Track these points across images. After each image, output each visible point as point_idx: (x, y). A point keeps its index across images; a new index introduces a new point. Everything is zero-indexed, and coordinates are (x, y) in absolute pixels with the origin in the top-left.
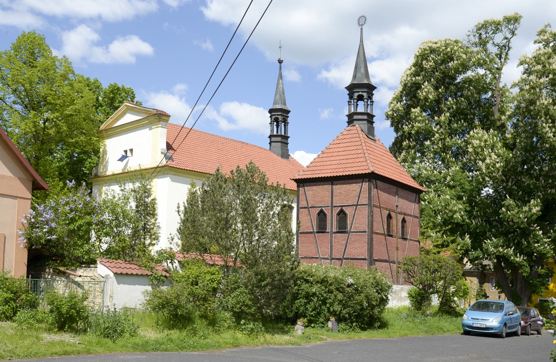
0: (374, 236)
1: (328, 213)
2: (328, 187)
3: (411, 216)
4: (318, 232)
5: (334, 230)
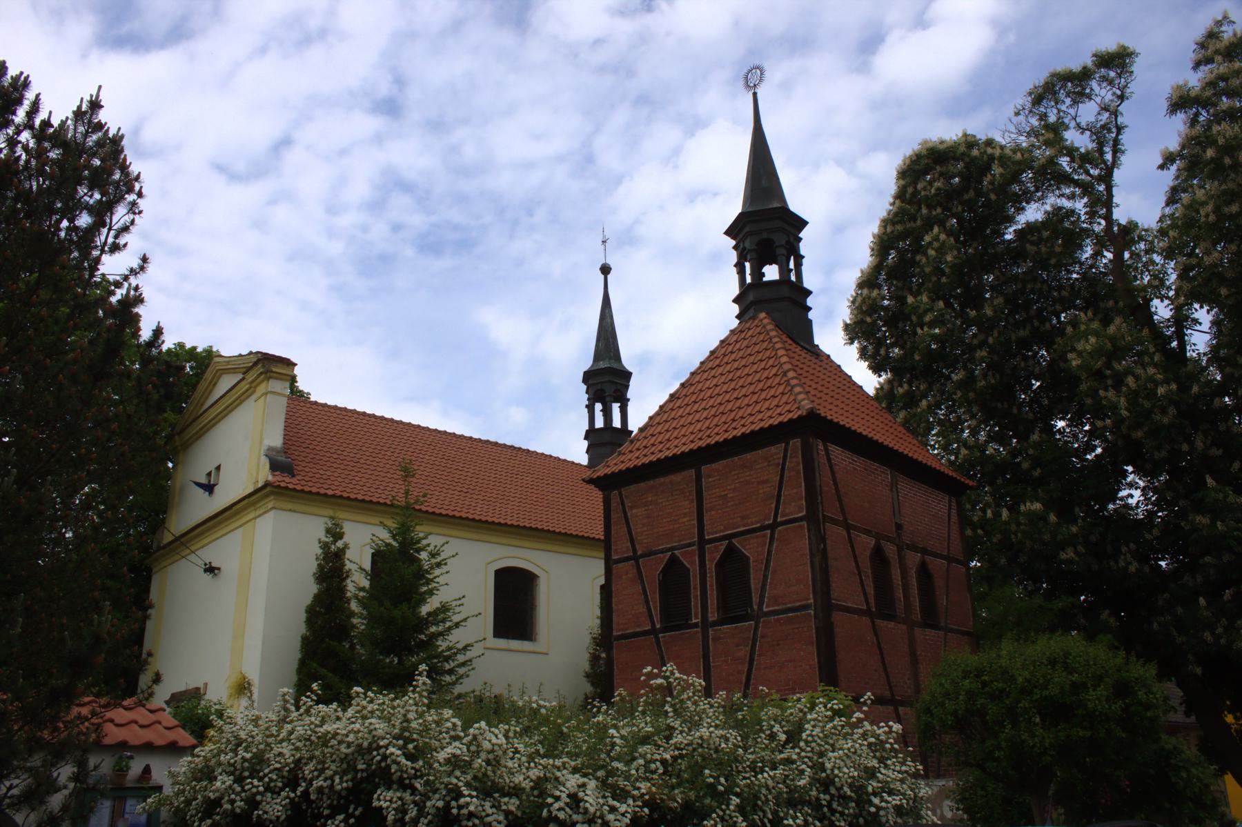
0: (837, 617)
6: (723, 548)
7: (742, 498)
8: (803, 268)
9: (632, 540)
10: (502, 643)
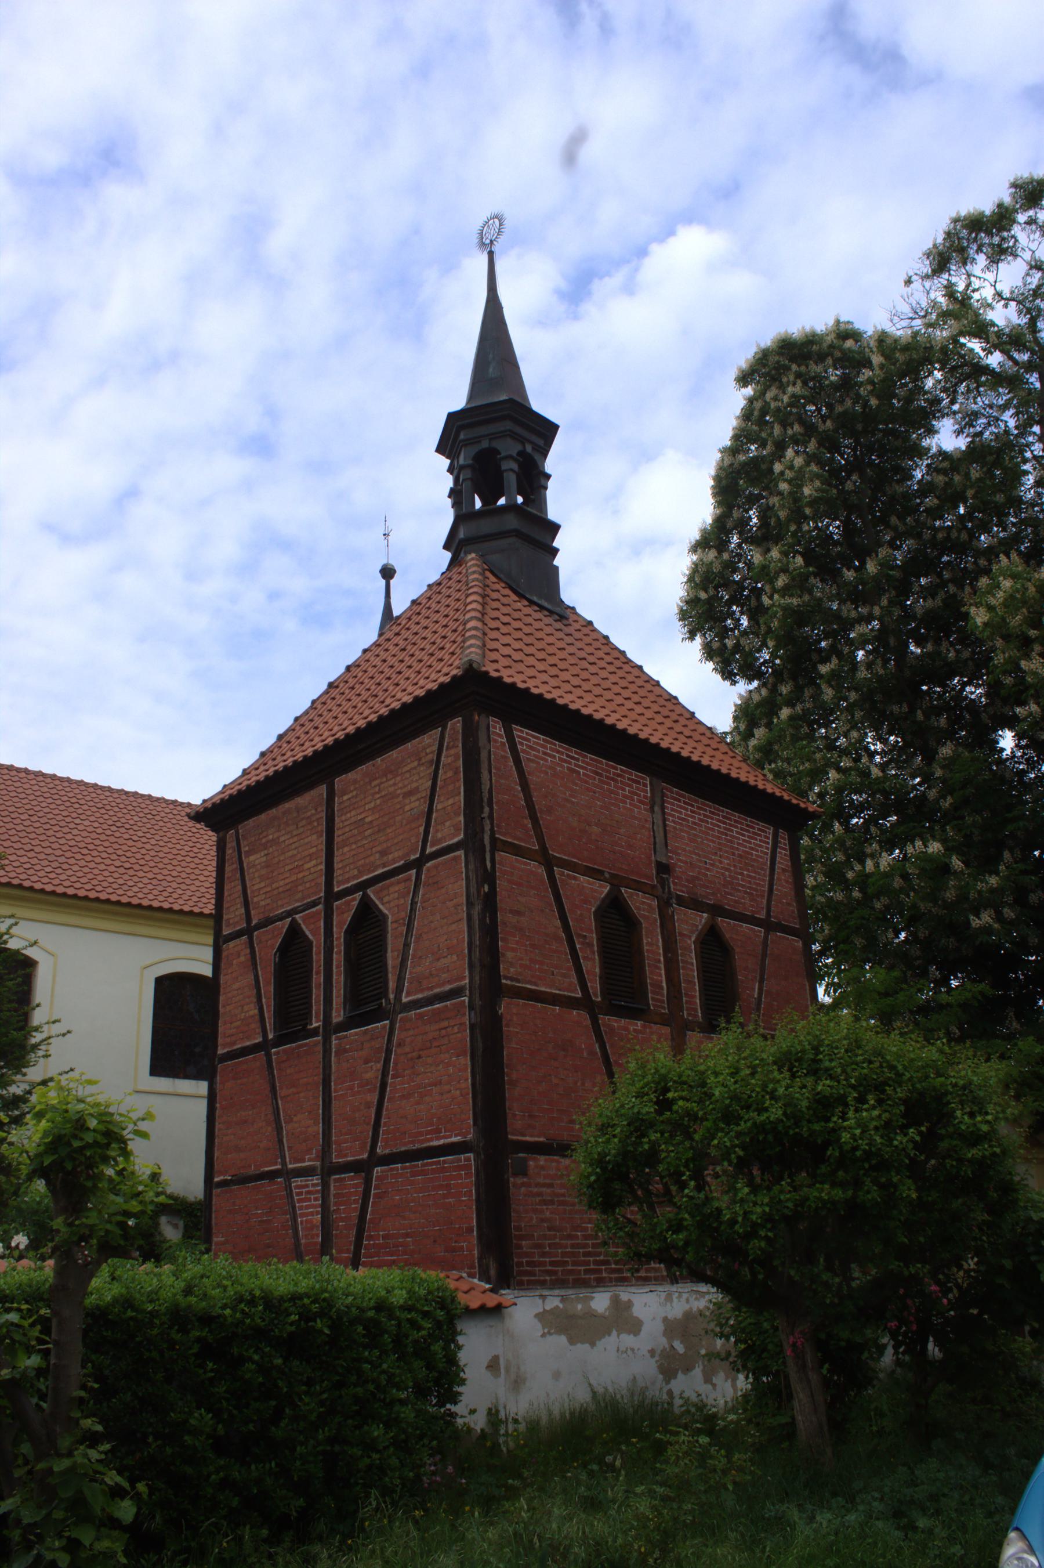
0: (507, 1008)
6: (356, 903)
9: (246, 904)
10: (164, 1084)
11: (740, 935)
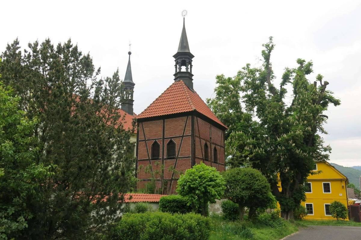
1: (161, 143)
2: (160, 122)
3: (219, 146)
4: (152, 159)
5: (165, 157)
7: (174, 129)
8: (192, 69)
11: (218, 148)
